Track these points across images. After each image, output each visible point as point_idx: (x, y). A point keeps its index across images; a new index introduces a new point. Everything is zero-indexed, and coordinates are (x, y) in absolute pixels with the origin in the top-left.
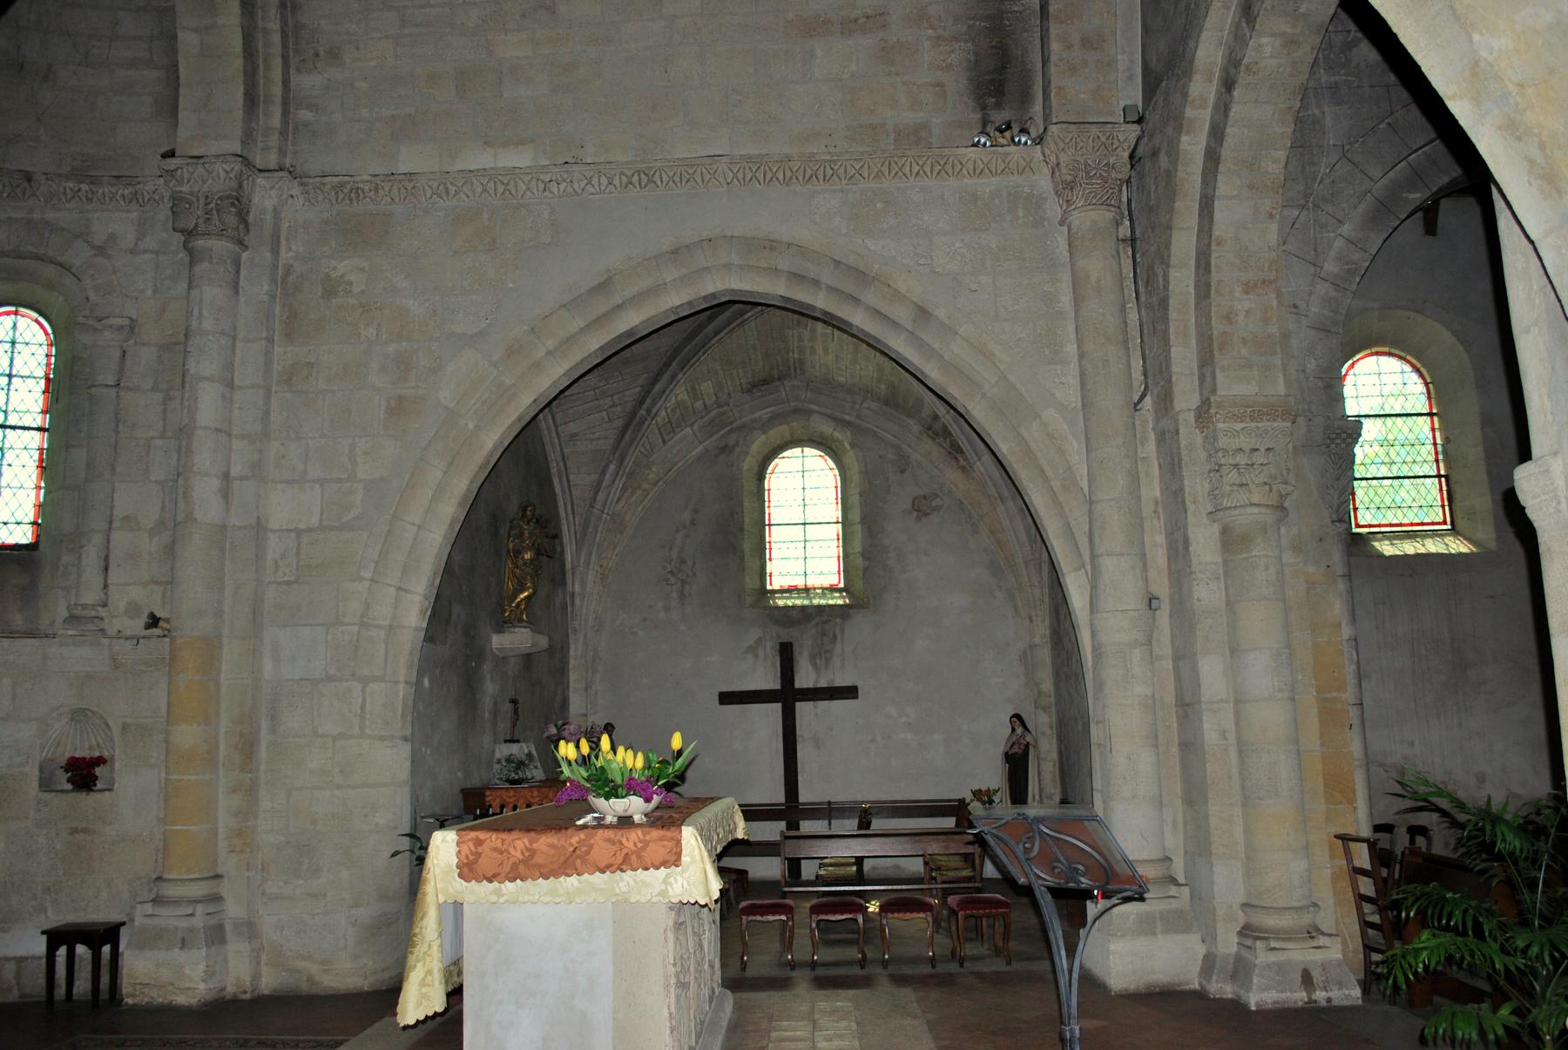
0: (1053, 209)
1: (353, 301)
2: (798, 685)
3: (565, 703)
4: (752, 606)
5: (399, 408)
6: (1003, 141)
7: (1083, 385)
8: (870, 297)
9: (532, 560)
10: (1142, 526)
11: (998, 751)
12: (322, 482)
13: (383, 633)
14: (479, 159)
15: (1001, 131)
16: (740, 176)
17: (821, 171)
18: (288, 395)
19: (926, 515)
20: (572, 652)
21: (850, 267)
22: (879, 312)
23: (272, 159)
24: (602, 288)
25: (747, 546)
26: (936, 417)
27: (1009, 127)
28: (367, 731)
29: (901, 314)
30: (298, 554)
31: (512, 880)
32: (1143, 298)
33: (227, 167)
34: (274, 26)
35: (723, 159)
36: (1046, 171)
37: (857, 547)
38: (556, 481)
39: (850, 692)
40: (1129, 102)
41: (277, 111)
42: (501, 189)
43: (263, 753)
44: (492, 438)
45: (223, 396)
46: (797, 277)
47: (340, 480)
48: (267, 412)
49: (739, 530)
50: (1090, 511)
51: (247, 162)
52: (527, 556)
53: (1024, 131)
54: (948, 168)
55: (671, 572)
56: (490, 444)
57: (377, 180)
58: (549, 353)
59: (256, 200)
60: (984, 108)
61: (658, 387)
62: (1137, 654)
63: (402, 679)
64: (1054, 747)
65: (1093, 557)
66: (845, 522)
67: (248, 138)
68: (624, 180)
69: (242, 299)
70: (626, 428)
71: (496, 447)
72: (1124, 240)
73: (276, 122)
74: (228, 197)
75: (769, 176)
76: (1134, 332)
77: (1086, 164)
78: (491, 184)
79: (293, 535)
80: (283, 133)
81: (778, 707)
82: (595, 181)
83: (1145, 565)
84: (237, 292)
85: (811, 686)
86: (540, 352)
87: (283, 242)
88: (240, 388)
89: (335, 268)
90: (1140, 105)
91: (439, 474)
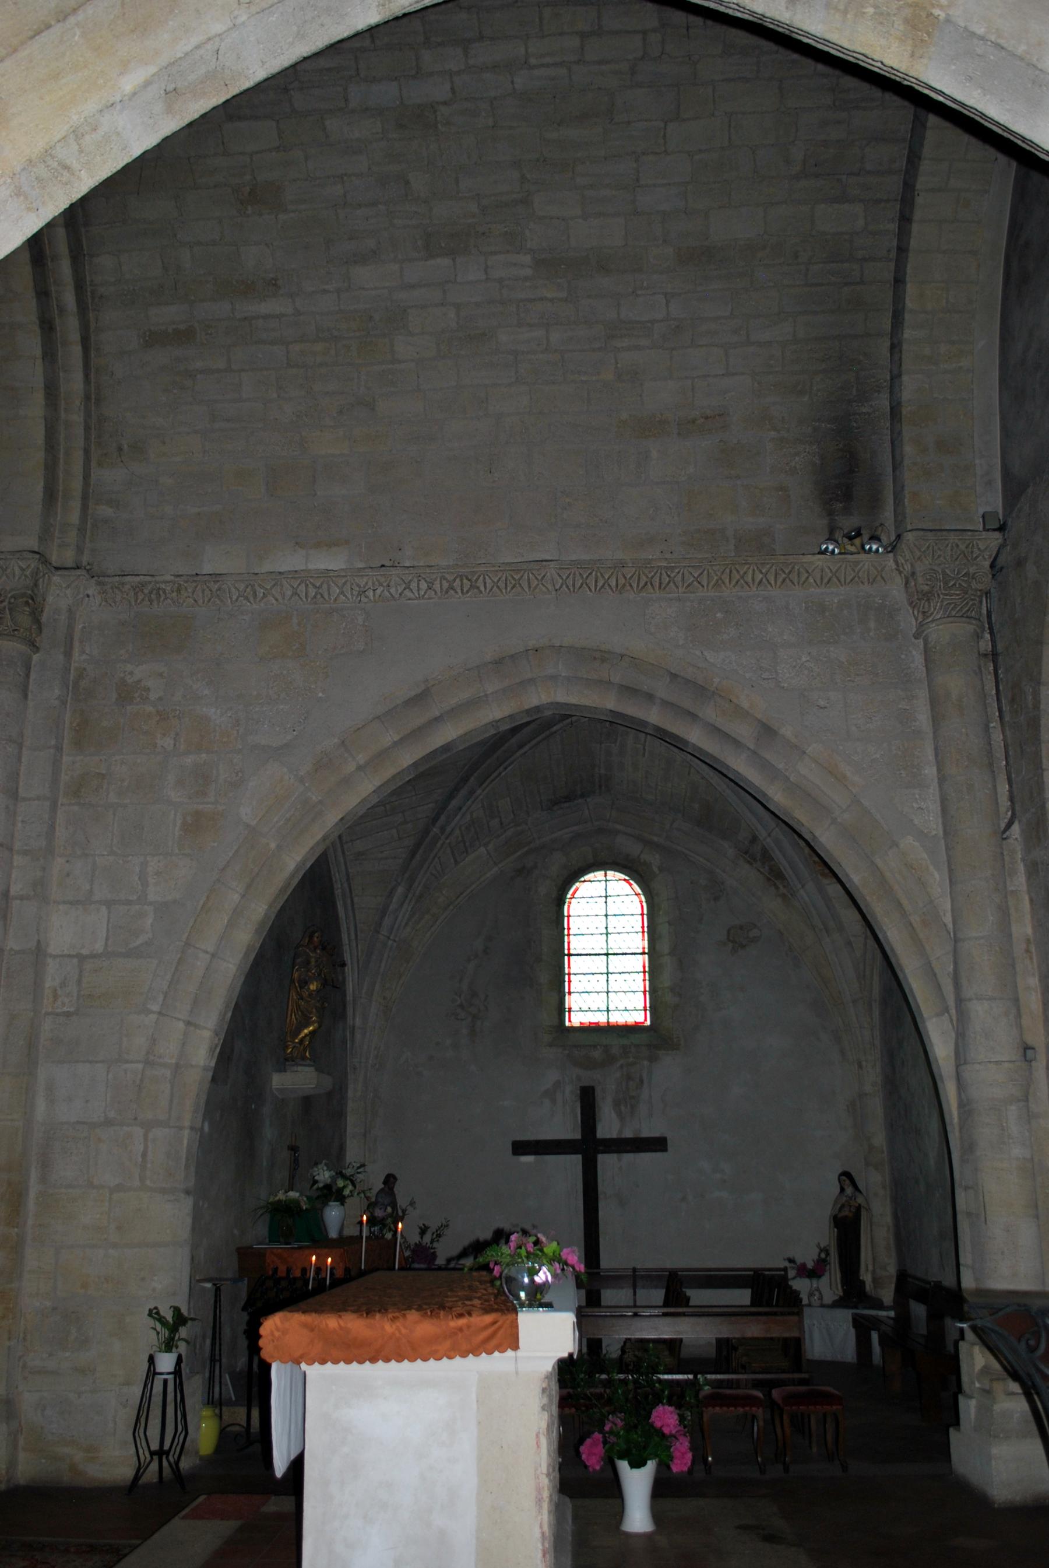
0: (908, 621)
1: (149, 709)
2: (600, 1135)
3: (342, 1148)
4: (551, 1045)
5: (196, 825)
6: (852, 549)
7: (944, 811)
8: (709, 713)
9: (318, 991)
10: (1013, 966)
11: (825, 1213)
12: (109, 904)
13: (168, 1073)
14: (290, 561)
15: (851, 538)
16: (570, 582)
17: (657, 579)
18: (76, 808)
19: (743, 947)
20: (350, 1094)
21: (688, 681)
22: (719, 730)
23: (69, 557)
24: (421, 698)
25: (544, 977)
26: (754, 839)
27: (859, 534)
28: (148, 1182)
29: (743, 731)
30: (79, 982)
31: (323, 1362)
32: (1007, 718)
33: (23, 565)
34: (77, 418)
35: (552, 565)
36: (899, 581)
37: (666, 980)
38: (340, 905)
39: (659, 1144)
40: (989, 509)
41: (76, 505)
42: (312, 592)
43: (31, 1204)
44: (294, 860)
45: (7, 807)
46: (629, 691)
47: (129, 903)
48: (52, 827)
49: (541, 957)
50: (955, 951)
51: (44, 560)
52: (313, 987)
53: (874, 538)
54: (794, 576)
55: (461, 1006)
56: (291, 866)
57: (180, 580)
58: (360, 768)
59: (50, 599)
60: (830, 513)
61: (454, 803)
62: (1013, 1111)
63: (187, 1123)
64: (888, 1210)
65: (959, 1001)
66: (653, 952)
67: (45, 535)
68: (446, 585)
69: (31, 704)
70: (418, 846)
71: (297, 869)
72: (985, 655)
73: (75, 517)
74: (23, 595)
75: (600, 584)
76: (999, 753)
77: (944, 573)
78: (303, 587)
79: (75, 961)
80: (81, 530)
81: (578, 1159)
82: (413, 585)
83: (1018, 1010)
84: (26, 696)
85: (614, 1135)
86: (351, 767)
87: (76, 644)
88: (24, 799)
89: (131, 673)
90: (1000, 511)
91: (236, 897)
